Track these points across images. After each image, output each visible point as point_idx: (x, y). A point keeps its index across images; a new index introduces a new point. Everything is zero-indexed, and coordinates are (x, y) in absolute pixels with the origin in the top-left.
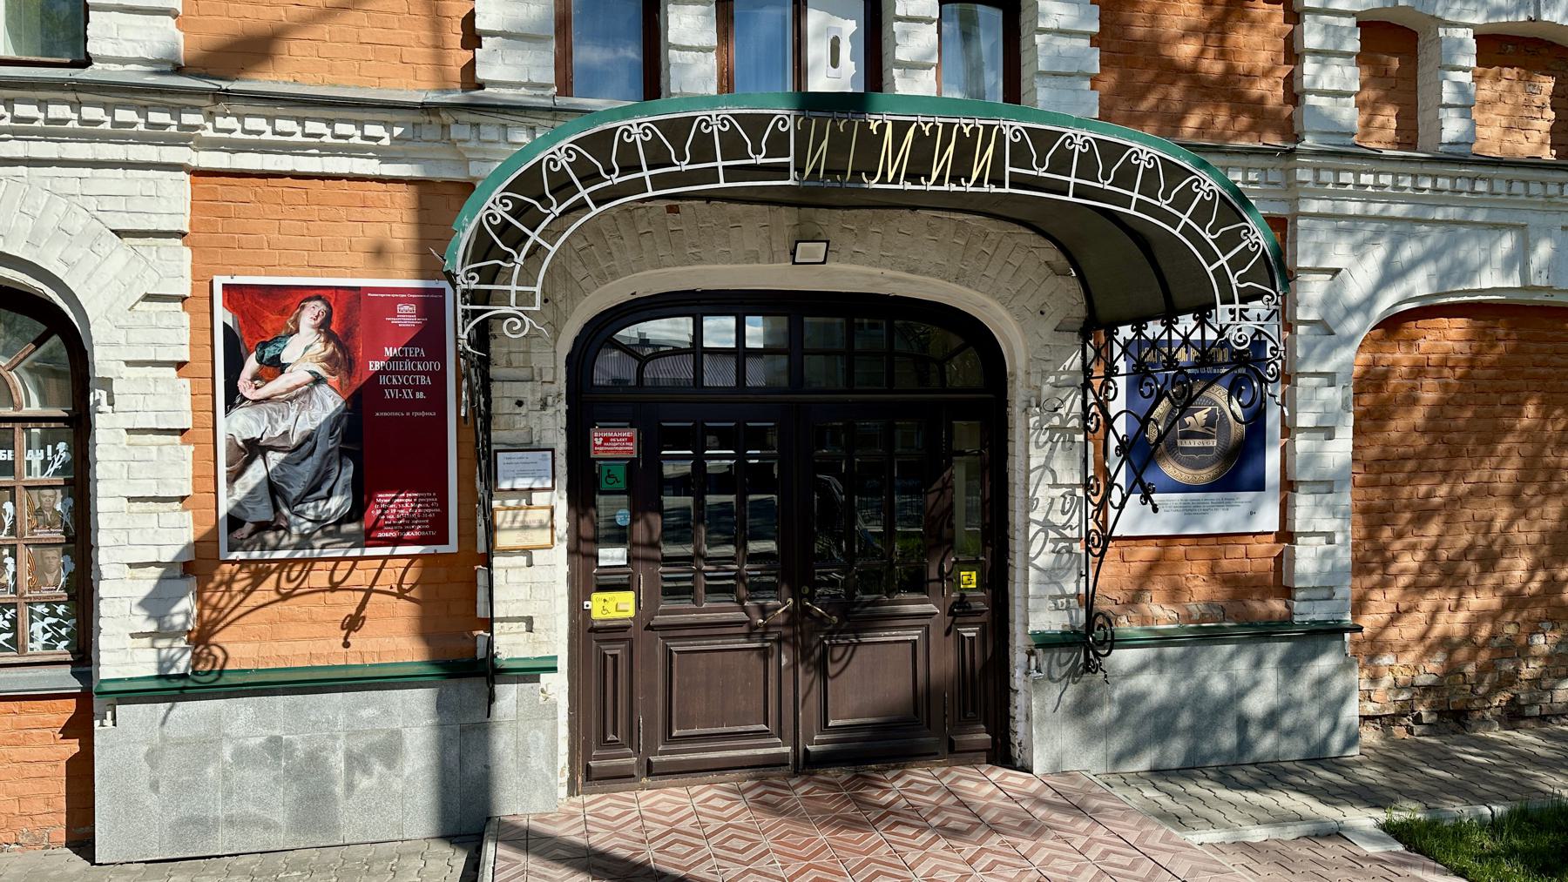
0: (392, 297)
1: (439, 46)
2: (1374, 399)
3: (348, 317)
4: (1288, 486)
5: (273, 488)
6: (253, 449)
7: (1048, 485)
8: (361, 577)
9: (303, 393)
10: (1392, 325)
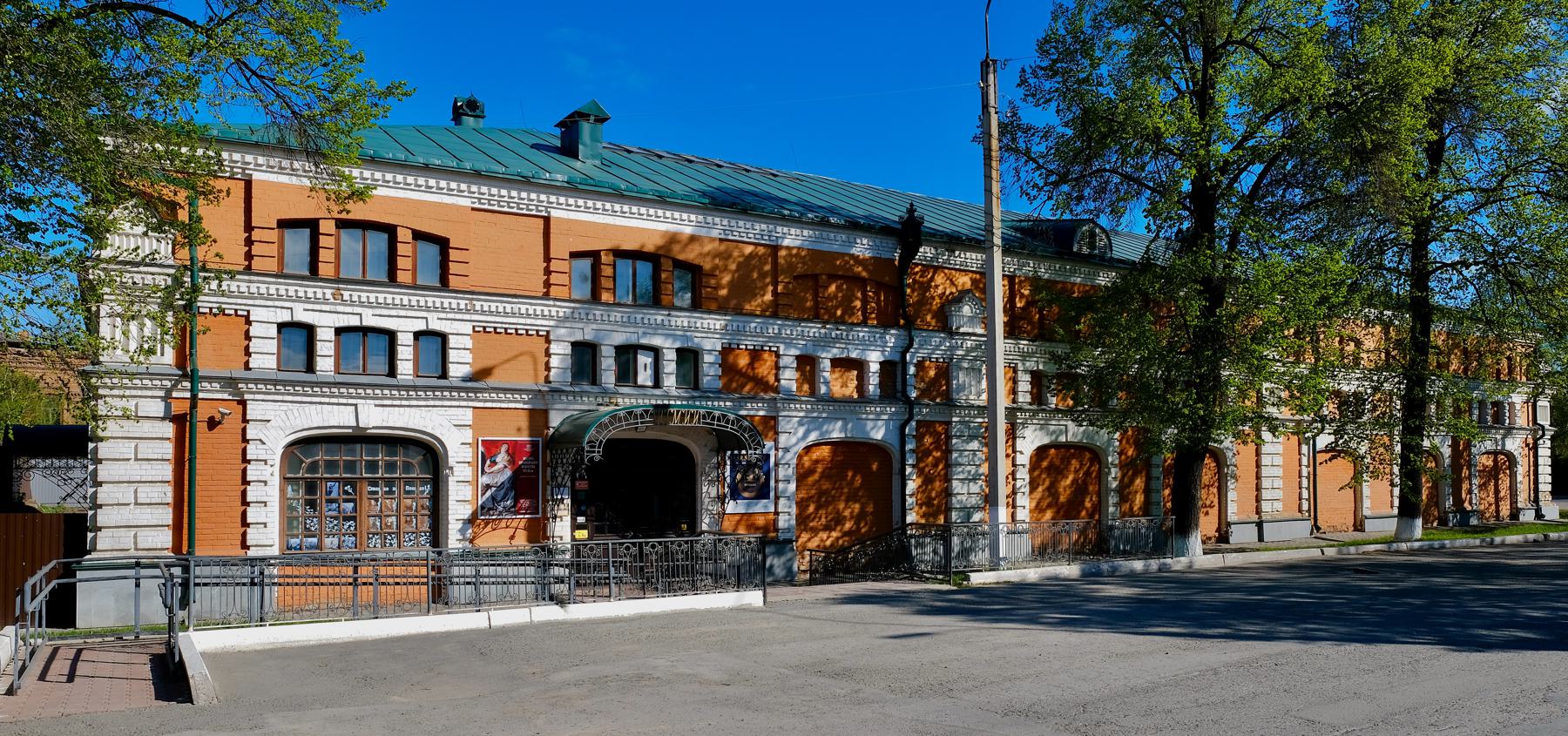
0: (523, 444)
1: (536, 370)
2: (802, 477)
3: (514, 448)
4: (777, 498)
5: (493, 498)
6: (488, 487)
7: (708, 491)
8: (514, 524)
9: (501, 471)
10: (808, 449)
